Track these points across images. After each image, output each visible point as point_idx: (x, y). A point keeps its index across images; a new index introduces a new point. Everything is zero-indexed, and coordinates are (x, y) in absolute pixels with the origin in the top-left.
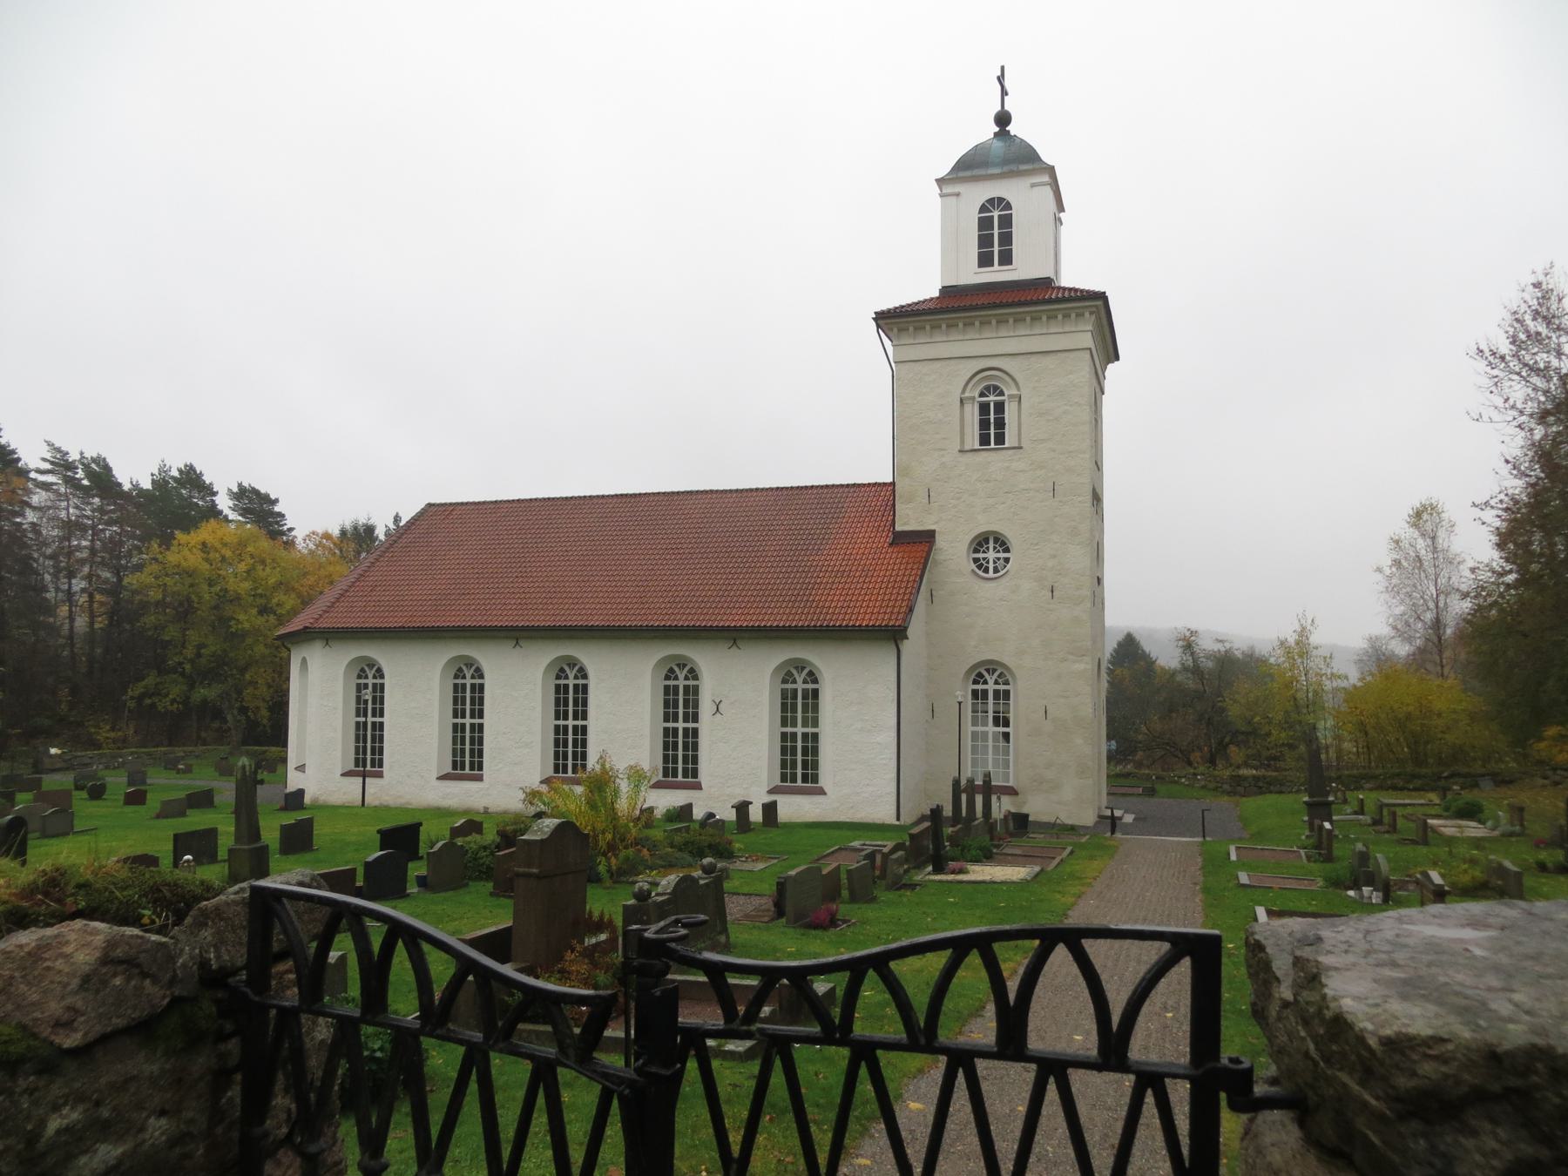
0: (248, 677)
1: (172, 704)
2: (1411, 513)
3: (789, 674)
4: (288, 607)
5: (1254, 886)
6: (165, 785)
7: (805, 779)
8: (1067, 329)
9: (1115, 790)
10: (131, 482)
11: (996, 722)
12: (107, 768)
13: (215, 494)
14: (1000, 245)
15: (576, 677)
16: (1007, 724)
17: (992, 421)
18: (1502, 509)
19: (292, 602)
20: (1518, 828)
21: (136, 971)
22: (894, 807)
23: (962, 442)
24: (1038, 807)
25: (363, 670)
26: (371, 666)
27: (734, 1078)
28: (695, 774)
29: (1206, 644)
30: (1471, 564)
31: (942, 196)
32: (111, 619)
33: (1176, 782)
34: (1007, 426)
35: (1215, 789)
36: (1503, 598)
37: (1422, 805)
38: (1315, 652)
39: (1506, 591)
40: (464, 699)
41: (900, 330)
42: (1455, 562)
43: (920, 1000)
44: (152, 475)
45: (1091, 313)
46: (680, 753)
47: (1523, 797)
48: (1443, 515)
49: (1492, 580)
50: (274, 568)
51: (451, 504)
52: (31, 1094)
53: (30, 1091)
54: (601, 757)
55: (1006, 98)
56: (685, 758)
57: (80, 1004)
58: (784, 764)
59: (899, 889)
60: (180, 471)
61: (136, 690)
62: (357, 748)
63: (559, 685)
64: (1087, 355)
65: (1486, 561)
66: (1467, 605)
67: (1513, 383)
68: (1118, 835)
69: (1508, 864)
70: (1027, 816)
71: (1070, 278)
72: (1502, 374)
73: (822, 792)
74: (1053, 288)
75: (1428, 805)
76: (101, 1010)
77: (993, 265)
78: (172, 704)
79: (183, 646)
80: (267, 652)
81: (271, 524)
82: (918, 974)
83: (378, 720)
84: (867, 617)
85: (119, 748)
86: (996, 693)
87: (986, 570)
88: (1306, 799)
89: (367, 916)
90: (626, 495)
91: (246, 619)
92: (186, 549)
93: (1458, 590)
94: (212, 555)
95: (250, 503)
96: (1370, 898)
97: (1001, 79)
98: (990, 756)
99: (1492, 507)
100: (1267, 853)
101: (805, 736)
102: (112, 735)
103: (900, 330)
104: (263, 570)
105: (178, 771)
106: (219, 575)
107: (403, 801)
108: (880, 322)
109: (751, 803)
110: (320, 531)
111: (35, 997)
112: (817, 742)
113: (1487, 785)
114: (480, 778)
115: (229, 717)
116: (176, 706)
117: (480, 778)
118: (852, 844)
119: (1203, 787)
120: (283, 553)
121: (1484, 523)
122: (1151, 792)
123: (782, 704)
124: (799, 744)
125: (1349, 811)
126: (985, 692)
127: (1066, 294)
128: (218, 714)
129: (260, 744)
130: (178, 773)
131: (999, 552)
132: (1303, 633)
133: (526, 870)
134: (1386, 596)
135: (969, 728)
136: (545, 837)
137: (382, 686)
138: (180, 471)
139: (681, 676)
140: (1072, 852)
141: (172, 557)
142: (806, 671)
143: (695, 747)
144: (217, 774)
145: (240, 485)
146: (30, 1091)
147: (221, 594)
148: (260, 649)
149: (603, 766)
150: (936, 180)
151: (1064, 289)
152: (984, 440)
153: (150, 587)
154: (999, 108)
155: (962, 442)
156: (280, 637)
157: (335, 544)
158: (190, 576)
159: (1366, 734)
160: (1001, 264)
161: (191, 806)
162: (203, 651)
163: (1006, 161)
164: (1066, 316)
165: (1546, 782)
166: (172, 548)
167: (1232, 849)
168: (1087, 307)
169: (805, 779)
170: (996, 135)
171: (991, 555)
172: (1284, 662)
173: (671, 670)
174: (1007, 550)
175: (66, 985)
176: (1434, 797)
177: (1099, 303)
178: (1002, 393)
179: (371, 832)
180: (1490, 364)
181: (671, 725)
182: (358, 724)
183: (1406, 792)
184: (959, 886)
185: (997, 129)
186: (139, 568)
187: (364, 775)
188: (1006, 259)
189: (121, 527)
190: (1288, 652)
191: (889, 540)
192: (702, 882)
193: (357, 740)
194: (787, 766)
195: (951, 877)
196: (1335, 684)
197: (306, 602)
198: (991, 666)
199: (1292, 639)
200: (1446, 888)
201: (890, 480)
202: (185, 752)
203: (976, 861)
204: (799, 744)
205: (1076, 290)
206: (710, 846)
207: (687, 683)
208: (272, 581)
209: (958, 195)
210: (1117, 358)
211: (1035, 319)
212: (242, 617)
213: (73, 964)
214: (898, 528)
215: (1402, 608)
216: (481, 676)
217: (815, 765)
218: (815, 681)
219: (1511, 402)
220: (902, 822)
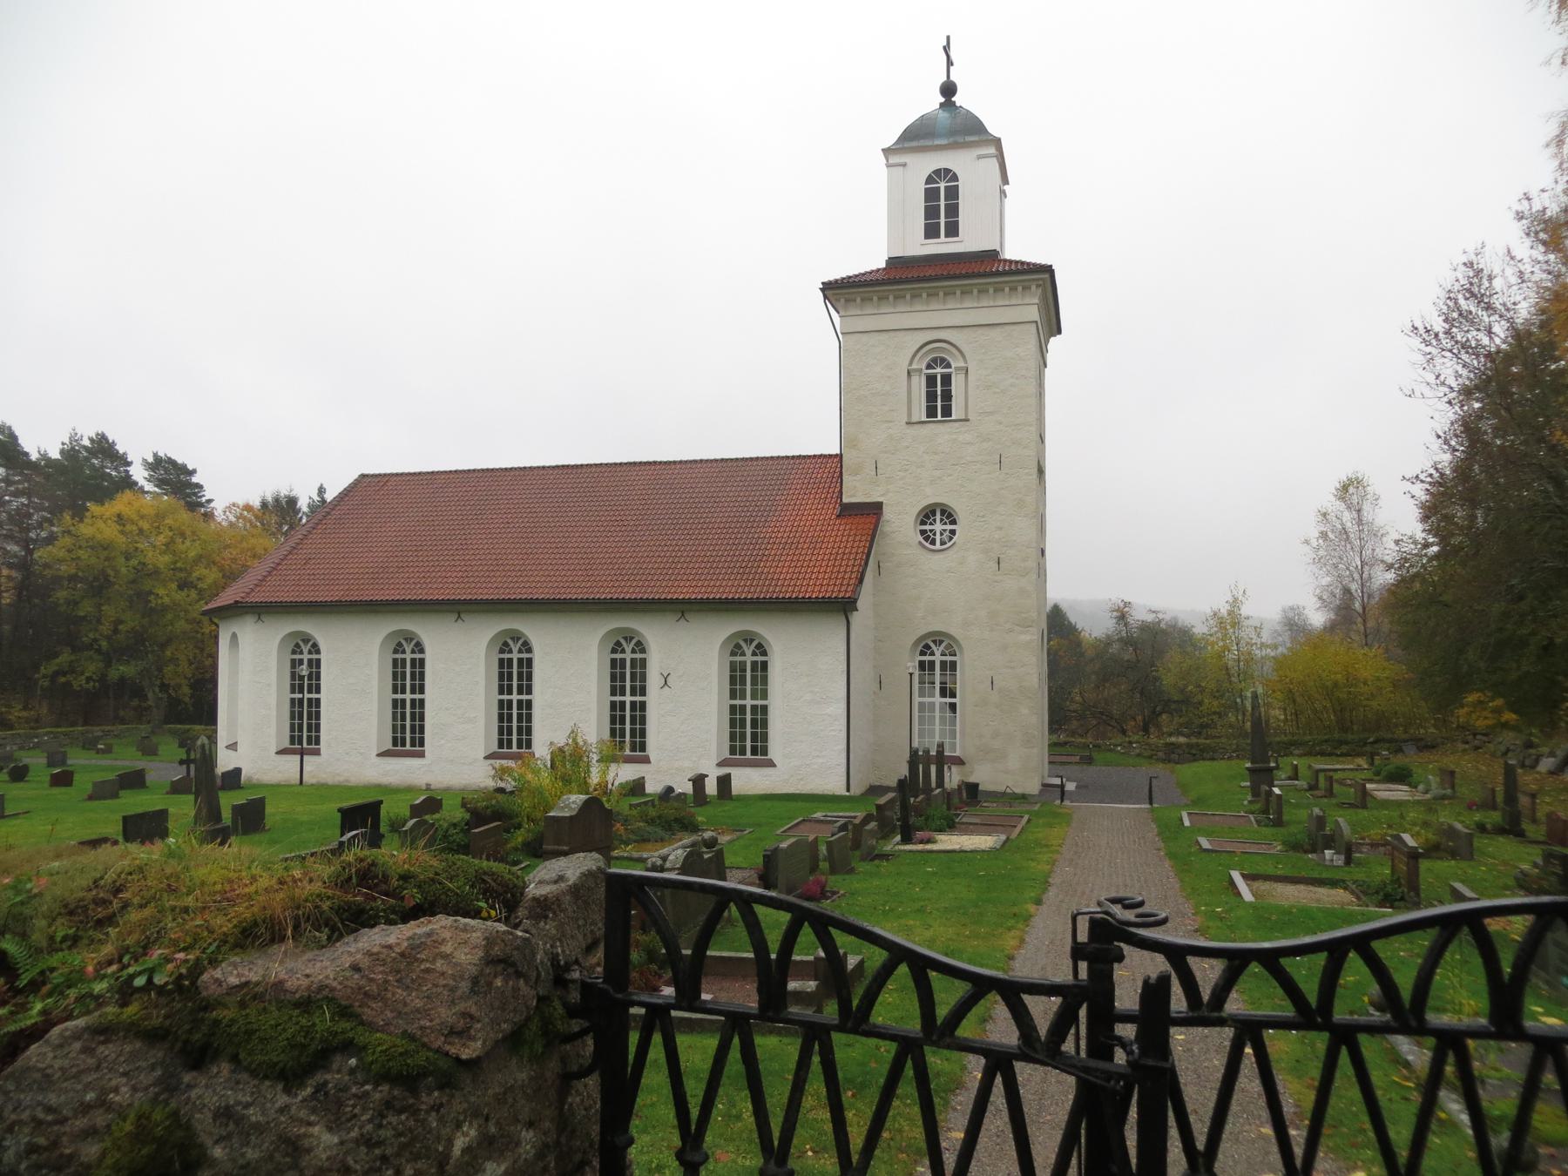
0: (168, 653)
1: (87, 682)
2: (1338, 486)
3: (738, 646)
4: (209, 581)
5: (1216, 851)
6: (89, 767)
7: (754, 751)
8: (1014, 302)
9: (1058, 759)
10: (39, 452)
11: (943, 693)
12: (21, 748)
13: (129, 464)
14: (946, 217)
15: (520, 651)
16: (953, 695)
17: (939, 393)
18: (1430, 483)
19: (213, 576)
20: (1449, 791)
21: (510, 970)
22: (845, 778)
23: (910, 414)
24: (986, 776)
25: (297, 645)
26: (306, 641)
27: (697, 1051)
28: (643, 747)
29: (1140, 615)
30: (1398, 537)
31: (888, 166)
32: (19, 596)
33: (1111, 750)
34: (953, 399)
35: (1150, 757)
36: (1426, 569)
37: (1352, 770)
38: (1246, 623)
39: (1429, 561)
40: (404, 674)
41: (847, 301)
42: (1379, 534)
43: (1405, 981)
44: (63, 444)
45: (1038, 286)
46: (628, 726)
47: (1449, 762)
48: (1369, 488)
49: (1416, 551)
50: (194, 541)
51: (385, 475)
52: (438, 1111)
53: (436, 1108)
54: (573, 732)
55: (951, 68)
56: (633, 731)
57: (474, 1010)
58: (733, 737)
59: (872, 860)
60: (91, 440)
61: (47, 669)
62: (292, 726)
63: (503, 659)
64: (1034, 325)
65: (1410, 534)
66: (1390, 577)
67: (1446, 360)
68: (1067, 803)
69: (1459, 826)
70: (976, 786)
71: (1014, 251)
72: (1434, 351)
73: (771, 764)
74: (1000, 261)
75: (1357, 770)
76: (491, 1015)
77: (939, 237)
78: (87, 682)
79: (99, 621)
80: (188, 627)
81: (188, 495)
82: (1403, 958)
83: (314, 696)
84: (830, 589)
85: (32, 728)
86: (943, 664)
87: (933, 542)
88: (1248, 765)
89: (755, 902)
90: (568, 466)
91: (166, 593)
92: (100, 523)
93: (1382, 561)
94: (129, 527)
95: (166, 473)
96: (1332, 860)
97: (946, 49)
98: (937, 727)
99: (1422, 481)
100: (1217, 818)
101: (754, 708)
102: (25, 714)
103: (847, 301)
104: (183, 543)
105: (98, 751)
106: (137, 548)
107: (341, 779)
108: (828, 293)
109: (707, 776)
110: (241, 503)
111: (418, 1003)
112: (767, 714)
113: (1410, 750)
114: (421, 755)
115: (150, 695)
116: (92, 684)
117: (421, 755)
118: (815, 816)
119: (1139, 755)
120: (203, 525)
121: (1413, 497)
122: (1089, 761)
123: (731, 676)
124: (748, 717)
125: (1283, 777)
126: (932, 663)
127: (1013, 267)
128: (139, 692)
129: (181, 723)
130: (98, 753)
131: (945, 523)
132: (1235, 602)
133: (556, 847)
134: (1314, 568)
135: (917, 699)
136: (574, 813)
137: (318, 661)
138: (91, 440)
139: (628, 649)
140: (1029, 821)
141: (85, 530)
142: (634, 642)
143: (643, 720)
144: (140, 753)
145: (155, 455)
146: (436, 1108)
147: (139, 568)
148: (181, 625)
149: (575, 740)
150: (883, 150)
151: (1011, 262)
152: (931, 412)
153: (60, 561)
154: (945, 79)
155: (910, 414)
156: (205, 613)
157: (256, 517)
158: (105, 549)
159: (1294, 701)
160: (946, 236)
161: (123, 787)
162: (120, 627)
163: (953, 132)
164: (1013, 289)
165: (1467, 746)
166: (86, 520)
167: (1184, 814)
168: (1034, 280)
169: (754, 752)
170: (942, 105)
171: (938, 527)
172: (1216, 632)
173: (618, 644)
174: (954, 522)
175: (453, 990)
176: (1362, 762)
177: (1047, 276)
178: (948, 366)
179: (331, 809)
180: (1424, 341)
181: (618, 698)
182: (293, 700)
183: (1334, 757)
184: (934, 856)
185: (943, 100)
186: (51, 539)
187: (302, 753)
188: (953, 230)
189: (29, 498)
190: (1221, 623)
191: (837, 511)
192: (706, 856)
193: (292, 718)
194: (736, 737)
195: (920, 847)
196: (1264, 653)
197: (230, 577)
198: (938, 638)
199: (1224, 612)
200: (1420, 851)
201: (839, 452)
202: (103, 731)
203: (941, 830)
204: (748, 717)
205: (1023, 263)
206: (676, 820)
207: (634, 656)
208: (192, 554)
209: (904, 165)
210: (1059, 331)
211: (983, 291)
212: (161, 592)
213: (456, 964)
214: (846, 500)
215: (1329, 579)
216: (422, 651)
217: (765, 738)
218: (764, 653)
219: (1442, 378)
220: (852, 792)
